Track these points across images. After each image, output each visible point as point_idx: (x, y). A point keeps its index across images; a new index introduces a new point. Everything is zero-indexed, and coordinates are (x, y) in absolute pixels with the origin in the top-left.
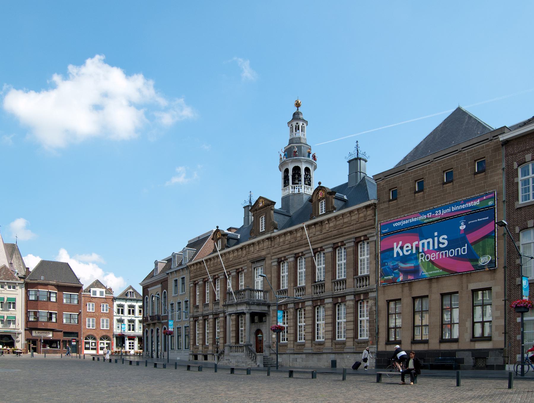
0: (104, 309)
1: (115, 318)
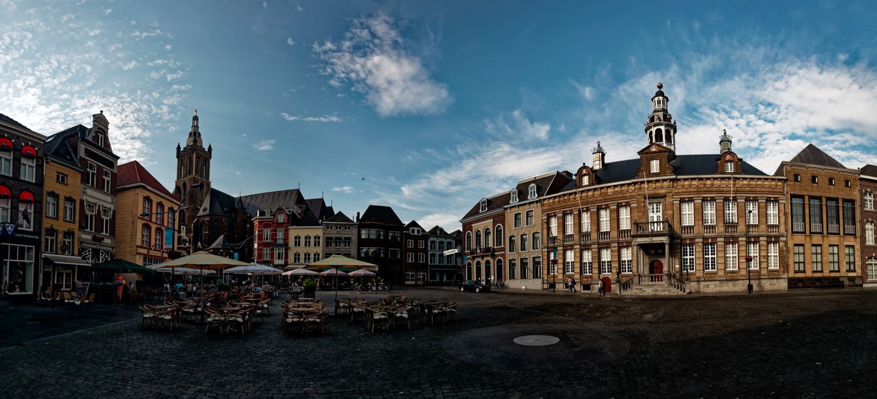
1: (429, 253)
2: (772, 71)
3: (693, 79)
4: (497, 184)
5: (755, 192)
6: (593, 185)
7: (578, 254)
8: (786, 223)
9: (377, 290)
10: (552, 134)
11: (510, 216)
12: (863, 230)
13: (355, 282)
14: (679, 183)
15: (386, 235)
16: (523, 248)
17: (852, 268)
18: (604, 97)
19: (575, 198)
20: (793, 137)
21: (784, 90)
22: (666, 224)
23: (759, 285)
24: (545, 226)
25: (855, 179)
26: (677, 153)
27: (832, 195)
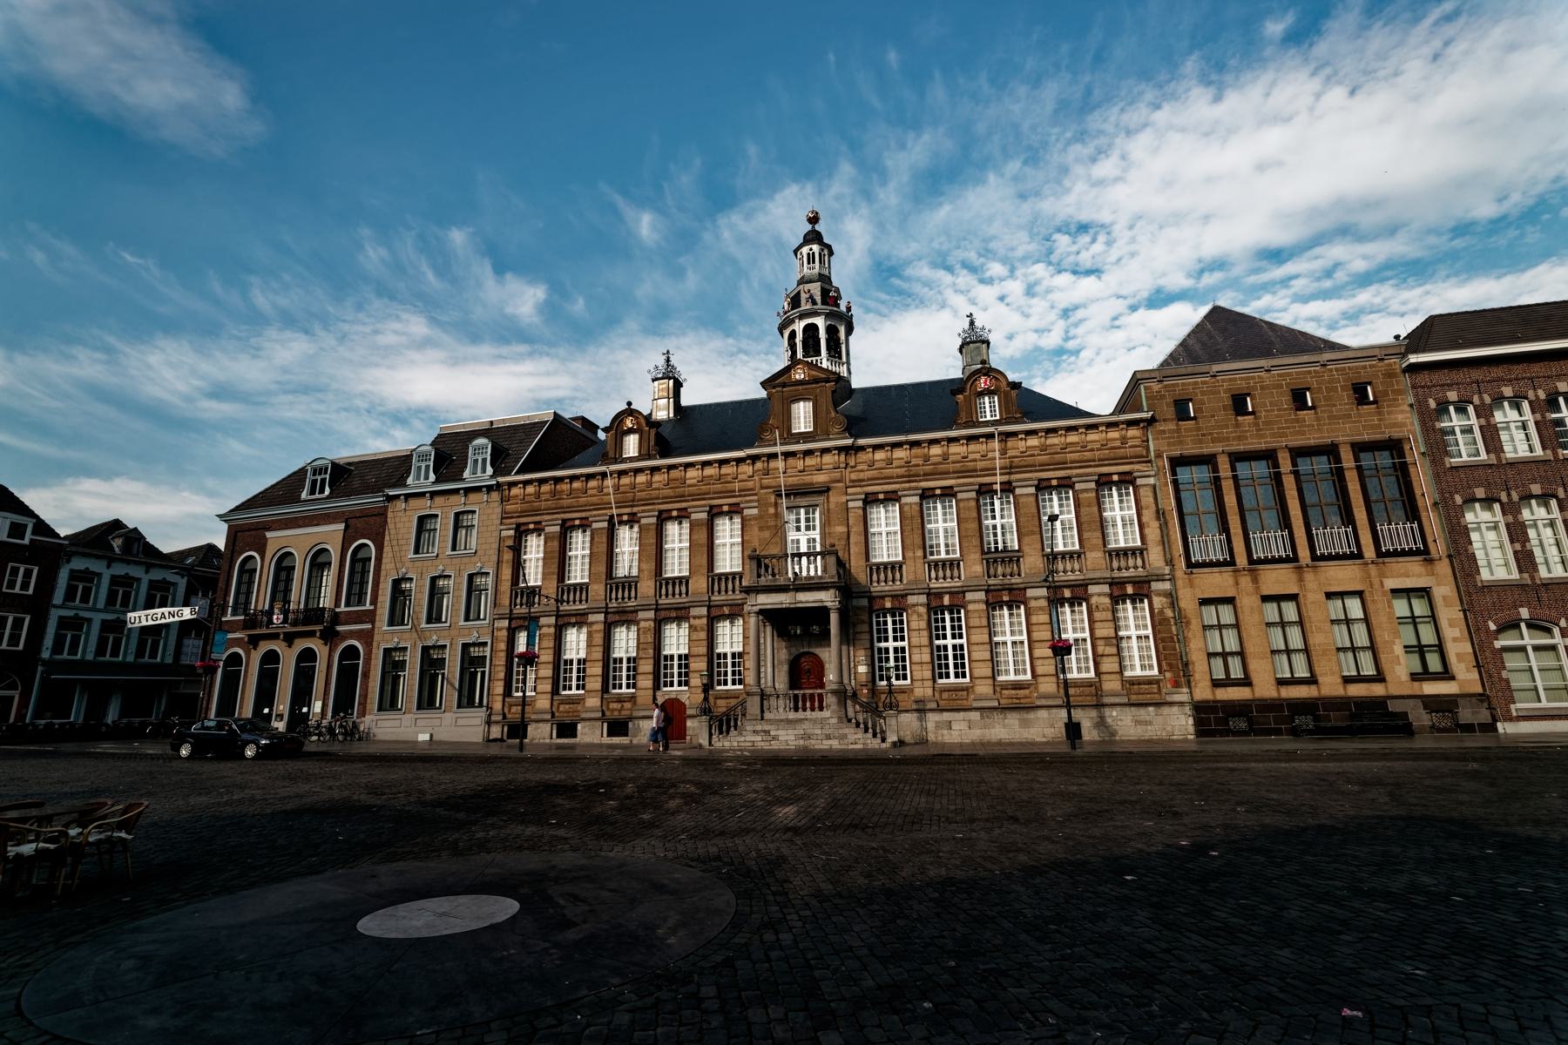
2: (1081, 137)
3: (890, 196)
4: (375, 424)
5: (1062, 464)
6: (650, 457)
7: (598, 639)
8: (1165, 541)
10: (551, 310)
11: (402, 521)
12: (1459, 536)
14: (862, 456)
16: (434, 616)
17: (1434, 663)
18: (684, 241)
19: (601, 489)
20: (1159, 299)
21: (1117, 180)
22: (832, 560)
23: (1101, 723)
24: (508, 556)
25: (1390, 375)
26: (856, 383)
27: (1312, 440)
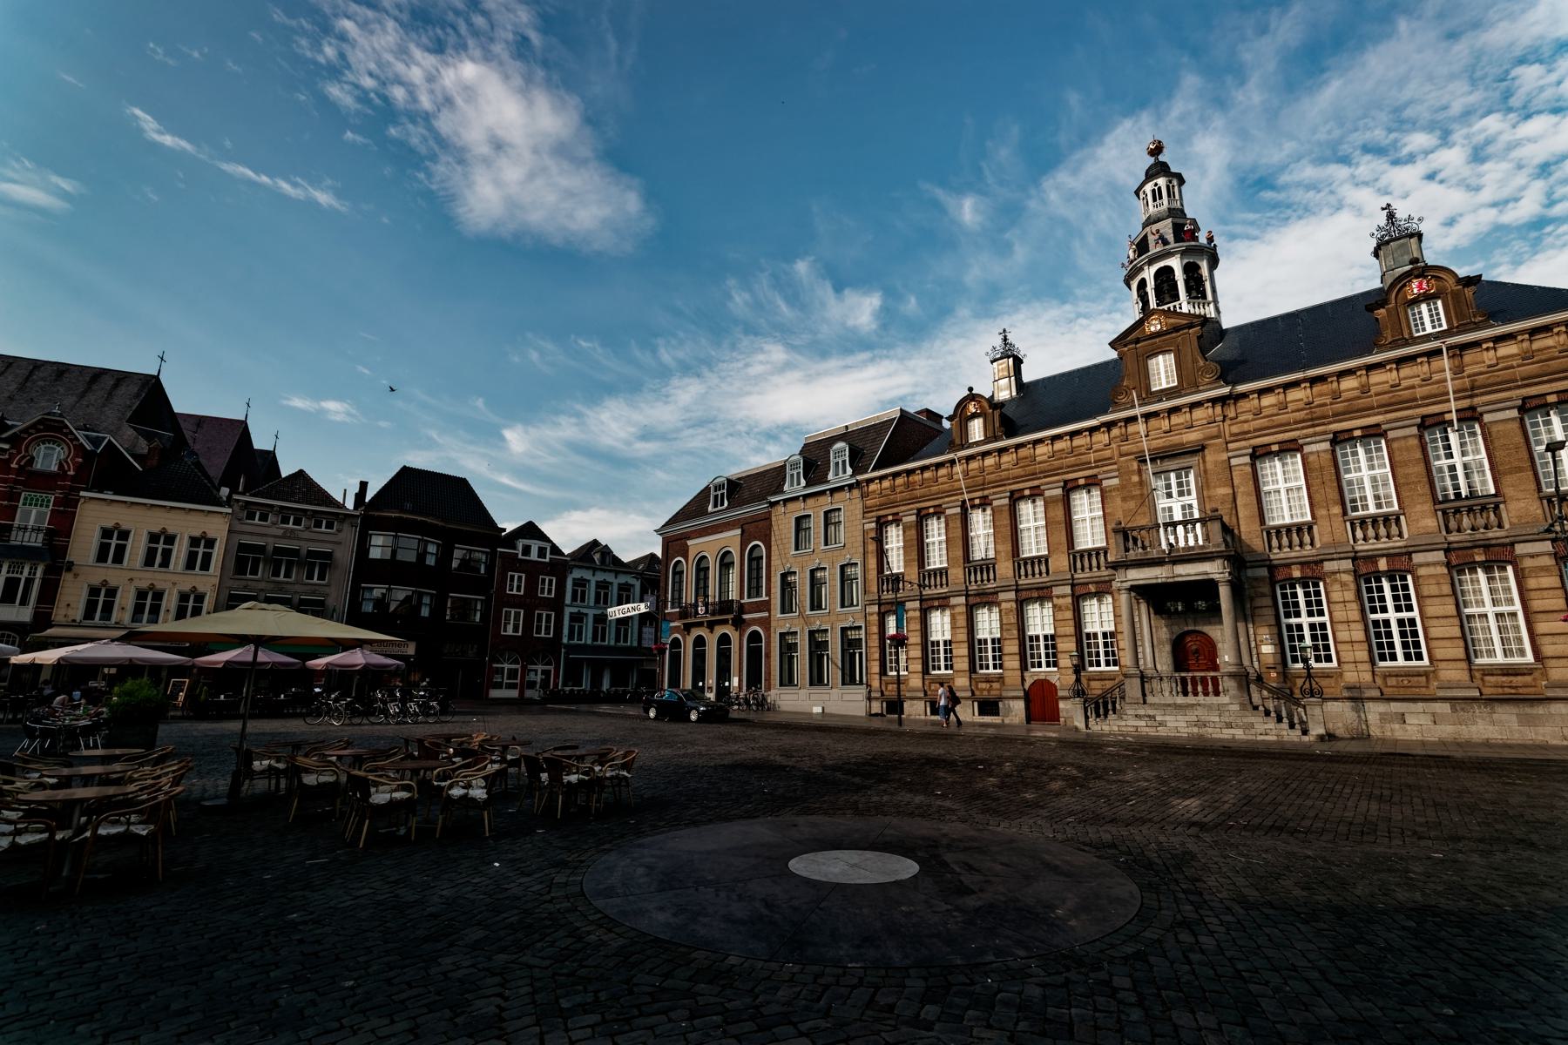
0: (547, 589)
1: (568, 611)
4: (753, 443)
6: (996, 439)
7: (962, 621)
9: (404, 711)
10: (887, 316)
13: (328, 690)
14: (1244, 405)
15: (445, 555)
16: (816, 604)
18: (1009, 214)
19: (950, 476)
22: (1215, 527)
24: (872, 547)
26: (1227, 322)
